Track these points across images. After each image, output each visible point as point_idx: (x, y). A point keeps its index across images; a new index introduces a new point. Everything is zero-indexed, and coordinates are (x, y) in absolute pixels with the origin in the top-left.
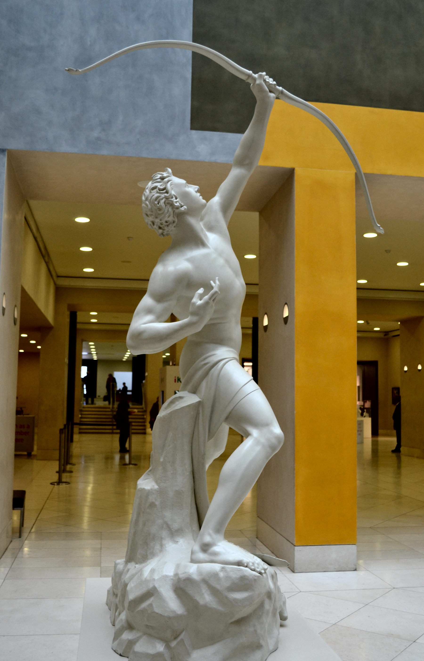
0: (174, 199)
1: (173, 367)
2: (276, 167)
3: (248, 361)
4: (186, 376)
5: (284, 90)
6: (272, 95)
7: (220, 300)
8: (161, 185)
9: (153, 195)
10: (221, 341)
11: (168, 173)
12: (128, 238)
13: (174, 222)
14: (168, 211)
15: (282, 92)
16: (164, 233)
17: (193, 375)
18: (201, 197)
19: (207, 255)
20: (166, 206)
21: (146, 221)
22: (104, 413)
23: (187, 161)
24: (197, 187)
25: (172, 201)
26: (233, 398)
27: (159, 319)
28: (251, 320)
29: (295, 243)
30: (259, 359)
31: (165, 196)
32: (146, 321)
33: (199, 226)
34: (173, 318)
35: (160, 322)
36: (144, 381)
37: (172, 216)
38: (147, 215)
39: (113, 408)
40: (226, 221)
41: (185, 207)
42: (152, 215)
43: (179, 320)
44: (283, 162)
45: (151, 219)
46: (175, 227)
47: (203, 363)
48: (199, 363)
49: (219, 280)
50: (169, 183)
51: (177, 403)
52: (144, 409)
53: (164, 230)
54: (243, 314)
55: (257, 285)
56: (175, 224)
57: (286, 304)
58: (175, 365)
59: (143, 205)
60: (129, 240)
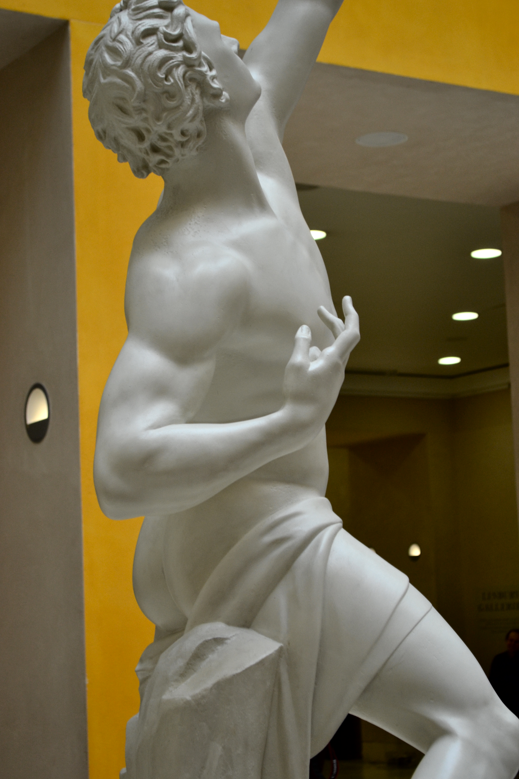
9: (150, 53)
13: (199, 135)
14: (193, 100)
20: (186, 86)
25: (203, 75)
31: (184, 57)
42: (144, 110)
47: (268, 539)
56: (201, 142)
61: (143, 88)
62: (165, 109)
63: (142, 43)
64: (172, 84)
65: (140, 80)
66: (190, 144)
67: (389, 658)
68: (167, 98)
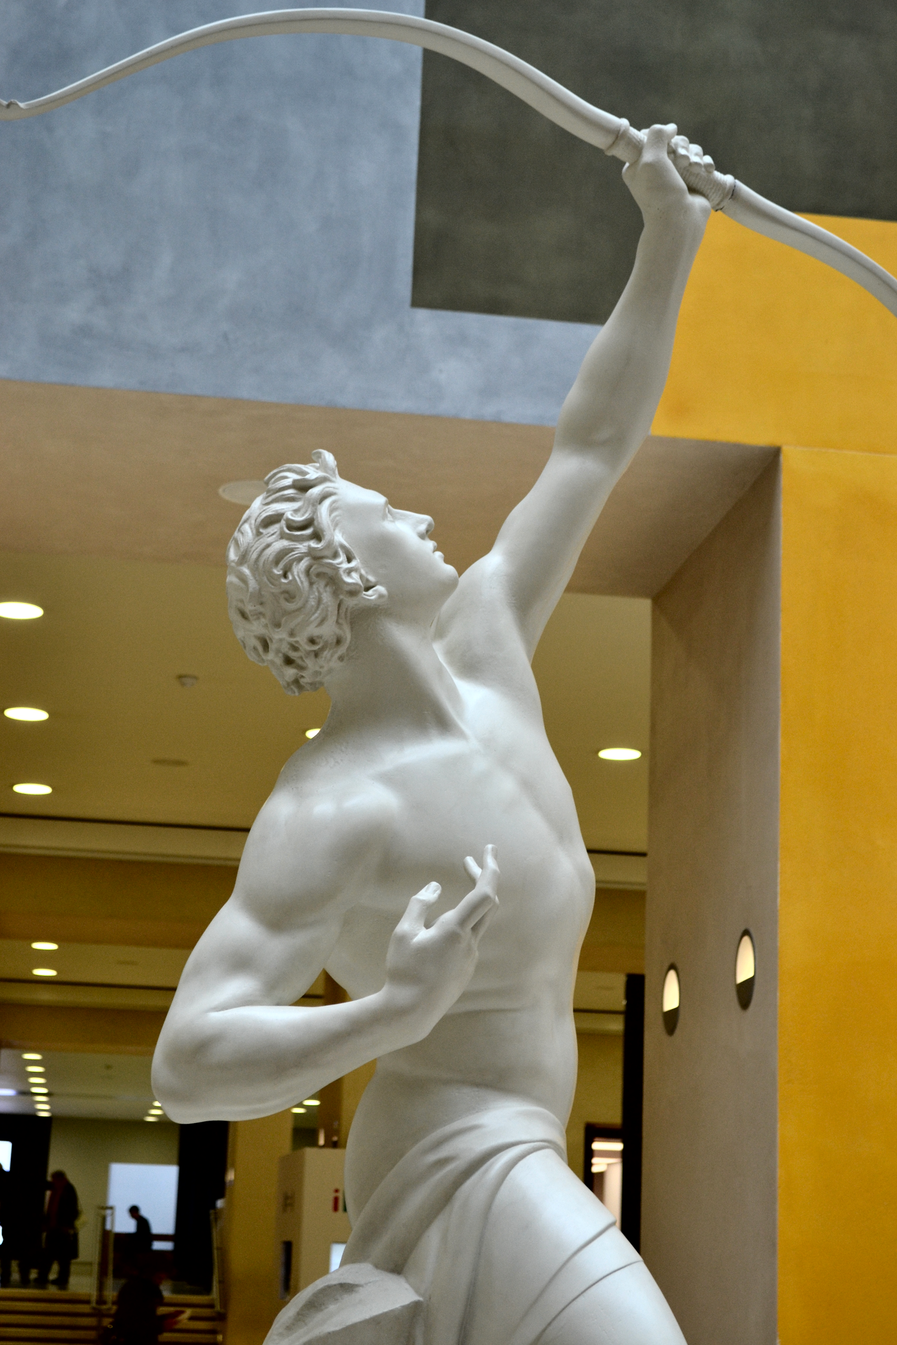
0: (341, 561)
1: (330, 1152)
2: (714, 443)
3: (608, 1133)
4: (368, 1208)
5: (739, 184)
6: (698, 202)
7: (497, 927)
8: (296, 511)
9: (268, 546)
10: (500, 1078)
11: (325, 467)
12: (180, 677)
13: (339, 642)
14: (319, 601)
15: (733, 193)
16: (302, 681)
17: (394, 1203)
18: (438, 554)
19: (454, 763)
20: (311, 584)
21: (240, 634)
22: (67, 1321)
23: (396, 415)
24: (424, 520)
25: (336, 569)
26: (536, 1301)
27: (272, 992)
28: (619, 982)
29: (782, 716)
30: (644, 1134)
32: (227, 999)
33: (428, 655)
34: (330, 992)
35: (278, 1004)
36: (220, 1203)
37: (332, 619)
38: (243, 615)
39: (101, 1301)
40: (527, 641)
41: (380, 589)
42: (261, 614)
43: (351, 1000)
44: (738, 424)
45: (257, 627)
46: (341, 658)
47: (432, 1158)
48: (417, 1157)
49: (496, 856)
50: (327, 502)
51: (332, 1307)
52: (218, 1308)
53: (302, 668)
54: (590, 959)
55: (643, 855)
56: (342, 650)
57: (746, 933)
58: (335, 1145)
59: (231, 579)
60: (183, 684)
61: (257, 587)
62: (286, 613)
63: (261, 533)
64: (291, 581)
65: (255, 578)
66: (325, 653)
67: (544, 1330)
68: (287, 600)
